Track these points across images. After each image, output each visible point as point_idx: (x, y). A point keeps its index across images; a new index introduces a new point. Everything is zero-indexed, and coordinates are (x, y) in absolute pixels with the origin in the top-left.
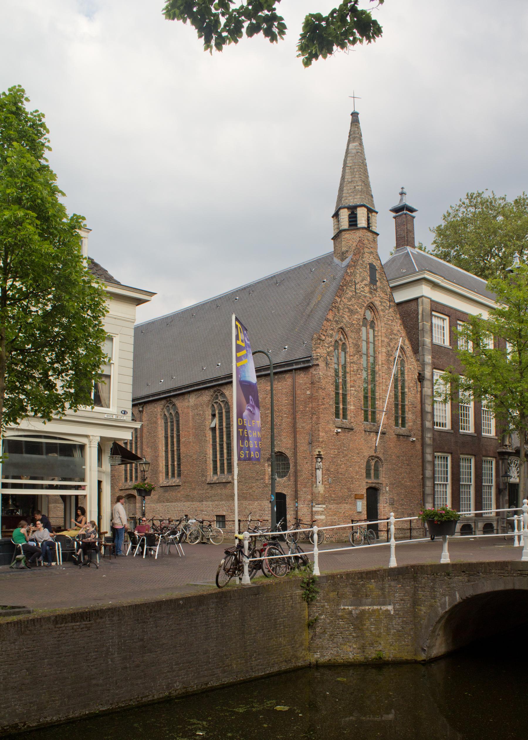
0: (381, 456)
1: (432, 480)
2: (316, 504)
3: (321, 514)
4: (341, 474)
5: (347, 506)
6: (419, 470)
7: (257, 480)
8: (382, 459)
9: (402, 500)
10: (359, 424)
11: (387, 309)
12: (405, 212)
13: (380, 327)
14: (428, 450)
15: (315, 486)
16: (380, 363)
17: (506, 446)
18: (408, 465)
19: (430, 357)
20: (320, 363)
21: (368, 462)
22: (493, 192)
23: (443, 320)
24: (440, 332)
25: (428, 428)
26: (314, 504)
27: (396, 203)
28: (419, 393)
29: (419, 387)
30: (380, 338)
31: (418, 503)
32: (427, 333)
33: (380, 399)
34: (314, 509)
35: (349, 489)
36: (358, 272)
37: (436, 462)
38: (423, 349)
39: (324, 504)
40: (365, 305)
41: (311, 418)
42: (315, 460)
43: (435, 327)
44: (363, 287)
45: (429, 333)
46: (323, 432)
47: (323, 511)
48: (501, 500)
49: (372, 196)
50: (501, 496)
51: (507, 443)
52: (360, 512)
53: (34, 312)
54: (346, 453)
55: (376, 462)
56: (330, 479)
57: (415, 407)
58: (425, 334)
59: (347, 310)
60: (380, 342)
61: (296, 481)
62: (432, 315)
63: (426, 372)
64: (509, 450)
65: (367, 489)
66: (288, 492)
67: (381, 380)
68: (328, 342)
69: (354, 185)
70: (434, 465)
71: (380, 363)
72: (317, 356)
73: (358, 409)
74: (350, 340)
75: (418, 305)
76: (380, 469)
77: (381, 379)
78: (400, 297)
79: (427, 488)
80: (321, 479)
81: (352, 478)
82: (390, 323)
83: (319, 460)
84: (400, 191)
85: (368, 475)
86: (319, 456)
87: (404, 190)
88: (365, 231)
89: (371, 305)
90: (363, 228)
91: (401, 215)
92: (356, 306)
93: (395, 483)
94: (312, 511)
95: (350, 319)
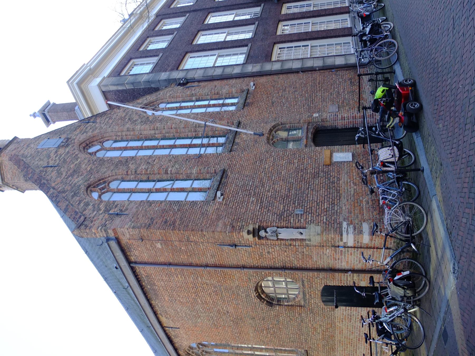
2: (341, 240)
4: (289, 190)
5: (344, 178)
6: (292, 77)
7: (302, 321)
8: (273, 124)
10: (220, 161)
11: (95, 126)
13: (111, 134)
14: (268, 67)
15: (307, 242)
16: (153, 132)
18: (285, 90)
19: (163, 73)
28: (201, 84)
30: (124, 134)
31: (335, 74)
33: (196, 131)
35: (315, 175)
39: (340, 224)
41: (196, 243)
45: (137, 77)
54: (257, 183)
57: (216, 86)
58: (138, 81)
59: (70, 178)
60: (128, 133)
63: (178, 77)
65: (316, 144)
66: (321, 281)
67: (174, 130)
71: (153, 132)
73: (198, 162)
74: (109, 173)
75: (110, 91)
77: (171, 131)
82: (111, 121)
83: (262, 233)
84: (32, 117)
87: (32, 113)
89: (84, 145)
93: (308, 105)
94: (355, 247)
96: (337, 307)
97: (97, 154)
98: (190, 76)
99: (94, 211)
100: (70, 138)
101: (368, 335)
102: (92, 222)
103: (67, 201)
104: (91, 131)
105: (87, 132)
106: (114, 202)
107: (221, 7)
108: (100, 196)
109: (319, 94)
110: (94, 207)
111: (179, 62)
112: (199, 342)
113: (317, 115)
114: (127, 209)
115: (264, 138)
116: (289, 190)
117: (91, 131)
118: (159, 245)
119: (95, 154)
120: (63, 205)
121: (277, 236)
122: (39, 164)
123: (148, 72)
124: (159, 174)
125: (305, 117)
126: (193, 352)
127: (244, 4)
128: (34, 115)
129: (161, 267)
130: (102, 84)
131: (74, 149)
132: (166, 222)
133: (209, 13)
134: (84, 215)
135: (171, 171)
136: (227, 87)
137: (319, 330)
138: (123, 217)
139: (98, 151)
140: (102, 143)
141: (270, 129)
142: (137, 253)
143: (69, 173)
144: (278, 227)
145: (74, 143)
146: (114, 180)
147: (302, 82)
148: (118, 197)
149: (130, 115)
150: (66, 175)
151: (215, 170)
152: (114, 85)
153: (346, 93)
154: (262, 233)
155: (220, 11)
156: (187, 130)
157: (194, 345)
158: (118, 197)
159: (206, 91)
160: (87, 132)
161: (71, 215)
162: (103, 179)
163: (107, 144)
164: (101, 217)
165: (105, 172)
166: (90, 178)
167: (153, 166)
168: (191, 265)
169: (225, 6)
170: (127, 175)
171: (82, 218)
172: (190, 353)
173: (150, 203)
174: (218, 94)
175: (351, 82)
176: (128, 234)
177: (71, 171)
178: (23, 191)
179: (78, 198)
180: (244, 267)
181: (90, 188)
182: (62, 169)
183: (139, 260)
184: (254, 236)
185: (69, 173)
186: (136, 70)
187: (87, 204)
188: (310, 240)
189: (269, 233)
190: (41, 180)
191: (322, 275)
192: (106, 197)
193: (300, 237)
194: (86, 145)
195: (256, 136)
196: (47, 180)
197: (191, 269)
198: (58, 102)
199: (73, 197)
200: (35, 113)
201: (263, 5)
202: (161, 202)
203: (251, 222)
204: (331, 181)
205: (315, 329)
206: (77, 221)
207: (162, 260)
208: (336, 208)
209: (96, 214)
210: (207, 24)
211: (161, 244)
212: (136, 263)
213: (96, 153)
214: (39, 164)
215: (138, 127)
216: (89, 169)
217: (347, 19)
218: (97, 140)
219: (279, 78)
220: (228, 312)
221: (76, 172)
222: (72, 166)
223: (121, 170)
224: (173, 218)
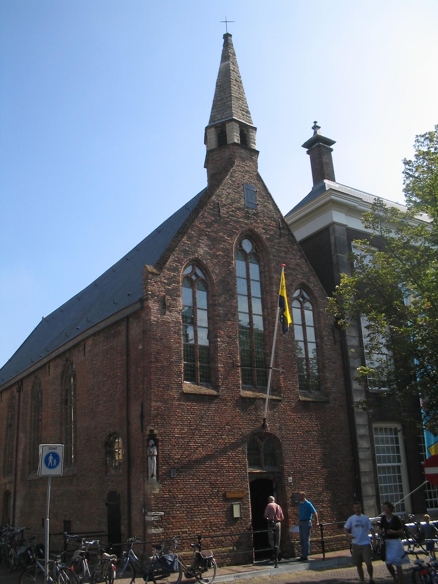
1: (371, 462)
16: (269, 305)
22: (227, 37)
27: (309, 135)
30: (267, 274)
35: (213, 485)
36: (225, 192)
44: (232, 211)
47: (157, 521)
49: (248, 112)
53: (301, 252)
68: (167, 276)
69: (224, 101)
74: (214, 277)
82: (282, 254)
92: (221, 234)
95: (211, 249)
96: (107, 504)
118: (140, 347)
149: (292, 274)
150: (209, 232)
153: (321, 510)
162: (206, 272)
172: (68, 362)
174: (324, 367)
184: (149, 435)
188: (148, 483)
193: (150, 475)
203: (161, 431)
204: (208, 500)
208: (178, 505)
209: (164, 283)
211: (141, 349)
220: (99, 404)
221: (214, 241)
224: (163, 359)
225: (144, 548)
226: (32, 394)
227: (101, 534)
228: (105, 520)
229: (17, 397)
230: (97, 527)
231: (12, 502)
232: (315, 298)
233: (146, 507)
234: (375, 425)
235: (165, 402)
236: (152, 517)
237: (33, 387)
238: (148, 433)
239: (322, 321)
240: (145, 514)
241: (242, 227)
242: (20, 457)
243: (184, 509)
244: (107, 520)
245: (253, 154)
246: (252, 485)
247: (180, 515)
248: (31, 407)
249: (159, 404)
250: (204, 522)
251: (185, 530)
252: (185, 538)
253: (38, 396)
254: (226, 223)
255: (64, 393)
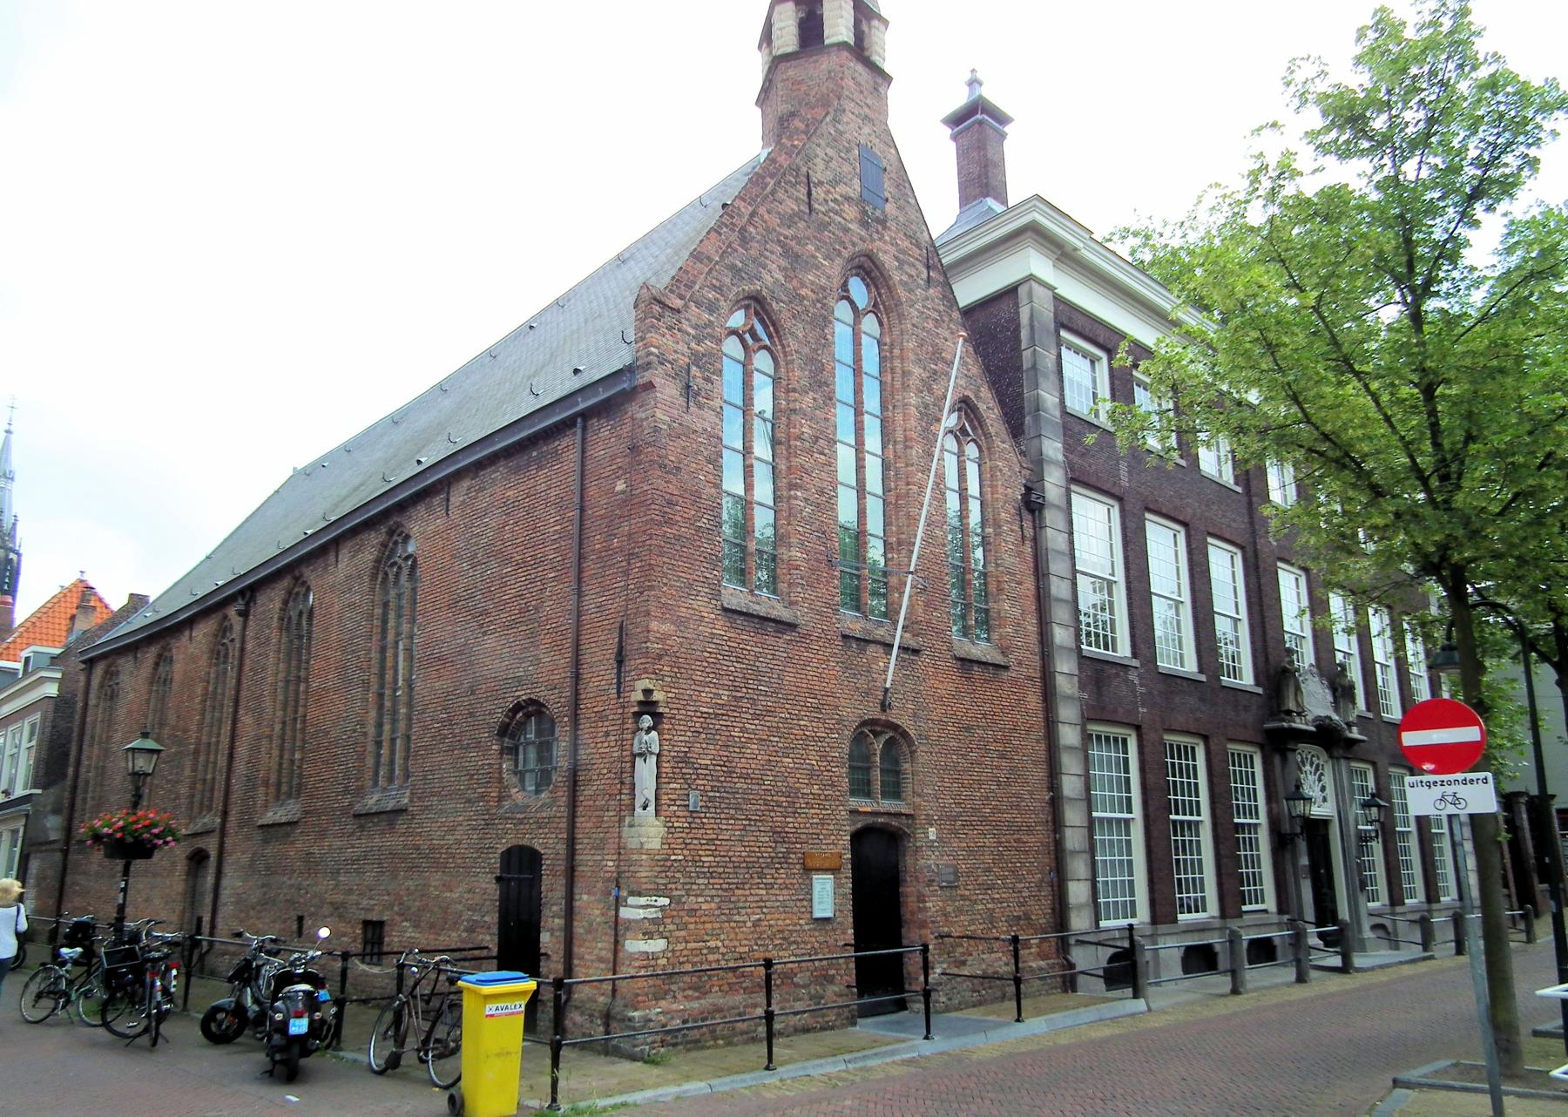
0: (905, 722)
1: (1084, 805)
2: (632, 893)
3: (649, 935)
4: (746, 777)
6: (1039, 774)
7: (469, 801)
9: (989, 870)
11: (918, 286)
12: (979, 116)
13: (896, 332)
15: (628, 819)
16: (899, 436)
17: (1289, 712)
18: (1002, 757)
20: (657, 381)
21: (859, 738)
23: (1092, 363)
24: (1081, 382)
25: (1061, 647)
26: (624, 893)
27: (959, 99)
28: (1028, 544)
29: (1028, 525)
31: (1042, 881)
32: (1046, 376)
34: (625, 913)
35: (779, 835)
37: (1095, 752)
38: (1037, 419)
40: (846, 254)
41: (626, 573)
42: (630, 724)
43: (1072, 391)
45: (1053, 378)
46: (663, 620)
47: (654, 921)
48: (1289, 867)
50: (1288, 856)
51: (1292, 705)
52: (827, 920)
54: (764, 702)
55: (890, 743)
56: (692, 794)
57: (1020, 583)
58: (1041, 380)
61: (573, 804)
62: (1059, 342)
63: (1047, 485)
64: (1299, 724)
66: (549, 845)
67: (903, 488)
70: (1087, 760)
72: (650, 354)
73: (817, 560)
74: (793, 345)
76: (907, 766)
77: (902, 484)
78: (970, 290)
79: (1068, 833)
80: (650, 794)
81: (793, 794)
83: (647, 721)
84: (968, 76)
85: (861, 787)
86: (647, 705)
87: (979, 76)
88: (845, 54)
89: (868, 264)
90: (843, 45)
91: (968, 128)
96: (499, 879)
97: (845, 302)
98: (1052, 518)
99: (696, 327)
100: (885, 228)
101: (213, 854)
102: (670, 328)
103: (721, 256)
104: (905, 278)
105: (900, 268)
106: (720, 373)
107: (1259, 578)
108: (734, 332)
109: (989, 841)
110: (706, 326)
111: (1093, 481)
112: (420, 560)
113: (932, 837)
114: (700, 407)
115: (874, 713)
116: (746, 777)
117: (905, 278)
118: (621, 486)
119: (843, 298)
120: (711, 249)
121: (641, 755)
122: (818, 160)
123: (1068, 403)
124: (789, 468)
125: (928, 807)
126: (396, 543)
127: (1265, 641)
128: (974, 82)
129: (576, 488)
130: (1035, 285)
131: (854, 245)
132: (670, 503)
133: (1242, 548)
134: (686, 306)
135: (796, 498)
136: (1017, 612)
137: (450, 839)
138: (682, 401)
139: (852, 303)
140: (875, 309)
141: (897, 727)
142: (605, 433)
143: (793, 243)
144: (658, 756)
145: (873, 241)
146: (775, 359)
147: (1023, 800)
148: (732, 374)
151: (796, 603)
152: (1032, 316)
154: (647, 721)
155: (1246, 575)
156: (903, 521)
157: (411, 549)
158: (732, 374)
159: (1009, 560)
160: (900, 268)
161: (687, 272)
162: (777, 332)
163: (870, 324)
164: (682, 347)
165: (797, 333)
166: (778, 301)
167: (810, 452)
168: (581, 557)
169: (1260, 590)
170: (788, 391)
171: (678, 303)
173: (715, 461)
175: (1019, 918)
176: (643, 415)
177: (797, 248)
178: (764, 98)
179: (727, 281)
180: (577, 677)
181: (757, 304)
182: (802, 225)
183: (590, 437)
184: (640, 703)
185: (793, 243)
186: (1075, 367)
187: (712, 308)
189: (646, 738)
190: (772, 176)
191: (562, 848)
192: (732, 347)
193: (639, 802)
194: (868, 269)
195: (880, 694)
196: (773, 193)
197: (572, 557)
198: (1007, 145)
199: (732, 267)
200: (980, 84)
201: (1260, 690)
202: (718, 486)
205: (452, 830)
206: (672, 291)
207: (592, 491)
210: (1206, 544)
211: (623, 492)
212: (584, 429)
213: (848, 299)
214: (818, 160)
215: (913, 400)
216: (803, 292)
217: (1204, 910)
218: (880, 295)
219: (1038, 741)
221: (795, 259)
222: (810, 247)
223: (799, 376)
225: (614, 990)
226: (281, 619)
227: (477, 953)
228: (492, 918)
229: (237, 628)
230: (464, 935)
231: (210, 880)
232: (987, 435)
233: (619, 886)
234: (1095, 728)
235: (680, 623)
236: (635, 910)
237: (286, 602)
238: (638, 696)
239: (1000, 490)
240: (618, 902)
241: (854, 245)
242: (240, 768)
243: (714, 892)
244: (496, 919)
245: (880, 80)
246: (857, 837)
247: (704, 907)
248: (279, 651)
249: (667, 628)
250: (756, 924)
251: (712, 944)
252: (714, 966)
253: (299, 624)
254: (824, 226)
255: (378, 611)
